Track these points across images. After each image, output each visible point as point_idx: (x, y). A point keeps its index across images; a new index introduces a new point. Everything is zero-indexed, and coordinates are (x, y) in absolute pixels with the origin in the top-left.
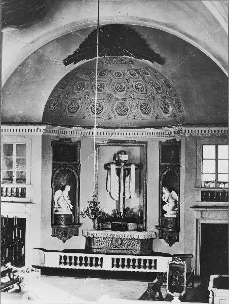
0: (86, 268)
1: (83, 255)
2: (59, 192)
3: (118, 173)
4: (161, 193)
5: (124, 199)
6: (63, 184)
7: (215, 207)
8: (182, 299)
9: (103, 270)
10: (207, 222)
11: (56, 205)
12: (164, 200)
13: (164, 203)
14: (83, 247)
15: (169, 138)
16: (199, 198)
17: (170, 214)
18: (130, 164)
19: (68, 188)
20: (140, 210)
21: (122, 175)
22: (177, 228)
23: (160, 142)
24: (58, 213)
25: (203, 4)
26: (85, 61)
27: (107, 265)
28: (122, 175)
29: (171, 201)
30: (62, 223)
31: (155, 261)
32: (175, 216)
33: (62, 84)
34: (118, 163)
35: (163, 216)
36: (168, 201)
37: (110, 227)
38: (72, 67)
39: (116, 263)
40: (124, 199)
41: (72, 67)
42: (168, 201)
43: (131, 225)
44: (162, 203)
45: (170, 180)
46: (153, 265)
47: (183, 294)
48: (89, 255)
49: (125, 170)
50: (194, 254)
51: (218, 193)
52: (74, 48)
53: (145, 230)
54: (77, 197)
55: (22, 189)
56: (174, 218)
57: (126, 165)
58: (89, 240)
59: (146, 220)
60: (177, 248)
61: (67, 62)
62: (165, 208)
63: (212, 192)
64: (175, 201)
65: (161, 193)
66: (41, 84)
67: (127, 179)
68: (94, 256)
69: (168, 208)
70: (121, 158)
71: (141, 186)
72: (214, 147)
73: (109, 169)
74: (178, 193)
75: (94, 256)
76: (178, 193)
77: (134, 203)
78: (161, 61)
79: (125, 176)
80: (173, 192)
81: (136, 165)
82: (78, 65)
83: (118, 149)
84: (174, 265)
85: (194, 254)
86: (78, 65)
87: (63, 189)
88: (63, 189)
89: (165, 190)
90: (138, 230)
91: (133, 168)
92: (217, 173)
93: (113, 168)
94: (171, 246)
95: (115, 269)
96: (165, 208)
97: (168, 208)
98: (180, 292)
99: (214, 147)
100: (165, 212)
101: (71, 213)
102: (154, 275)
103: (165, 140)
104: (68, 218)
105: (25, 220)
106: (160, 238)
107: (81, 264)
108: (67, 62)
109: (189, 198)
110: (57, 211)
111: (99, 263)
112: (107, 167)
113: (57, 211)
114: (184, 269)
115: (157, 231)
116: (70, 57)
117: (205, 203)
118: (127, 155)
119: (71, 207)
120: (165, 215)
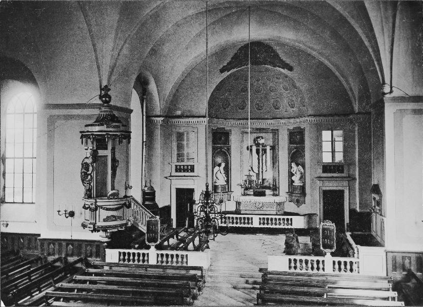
1: (235, 216)
2: (217, 168)
4: (290, 167)
5: (262, 172)
9: (253, 227)
10: (328, 189)
11: (215, 178)
13: (293, 175)
14: (234, 209)
15: (295, 126)
16: (320, 171)
19: (223, 165)
21: (261, 154)
22: (303, 193)
24: (217, 184)
26: (235, 70)
27: (256, 224)
29: (298, 173)
32: (302, 184)
33: (218, 88)
34: (258, 145)
36: (296, 173)
37: (252, 193)
38: (226, 74)
40: (262, 172)
41: (226, 74)
42: (296, 173)
43: (268, 192)
44: (291, 175)
45: (296, 156)
48: (238, 216)
49: (262, 150)
50: (318, 213)
56: (300, 186)
57: (263, 146)
58: (238, 203)
60: (304, 209)
62: (293, 178)
64: (301, 173)
65: (290, 167)
66: (220, 4)
67: (264, 156)
69: (296, 178)
70: (259, 142)
72: (330, 131)
73: (251, 150)
78: (290, 69)
82: (229, 73)
83: (255, 135)
85: (318, 213)
86: (229, 73)
87: (219, 165)
88: (219, 165)
89: (293, 165)
90: (274, 195)
95: (262, 226)
96: (293, 178)
97: (296, 178)
99: (330, 131)
101: (226, 183)
102: (290, 230)
104: (223, 188)
105: (194, 166)
109: (312, 172)
110: (216, 182)
111: (250, 221)
112: (250, 149)
113: (216, 182)
115: (287, 196)
118: (264, 140)
119: (226, 178)
120: (294, 184)
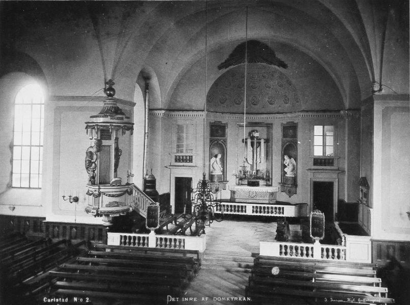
0: (235, 213)
1: (229, 204)
2: (213, 159)
3: (252, 145)
6: (216, 153)
7: (323, 169)
8: (322, 242)
10: (318, 180)
11: (212, 168)
12: (286, 164)
13: (285, 167)
14: (229, 197)
17: (289, 174)
18: (260, 140)
19: (220, 156)
20: (268, 171)
21: (255, 147)
23: (282, 124)
24: (213, 174)
25: (133, 91)
27: (249, 212)
28: (255, 147)
29: (290, 165)
30: (216, 181)
31: (283, 208)
34: (252, 138)
35: (284, 175)
36: (288, 165)
37: (246, 183)
39: (255, 209)
41: (224, 70)
42: (288, 165)
43: (261, 182)
45: (289, 149)
46: (281, 211)
47: (322, 238)
48: (233, 204)
49: (257, 143)
50: (309, 204)
51: (325, 159)
52: (226, 57)
53: (271, 185)
54: (225, 162)
55: (189, 156)
56: (292, 177)
58: (233, 193)
59: (272, 179)
61: (220, 68)
62: (286, 170)
63: (321, 159)
64: (294, 166)
67: (258, 149)
68: (237, 204)
69: (288, 170)
71: (268, 154)
73: (246, 143)
74: (296, 160)
75: (237, 204)
76: (296, 160)
77: (262, 167)
78: (284, 65)
79: (257, 148)
80: (292, 159)
81: (265, 140)
82: (227, 69)
84: (316, 216)
85: (309, 204)
87: (216, 156)
89: (286, 157)
90: (267, 185)
91: (262, 141)
92: (40, 146)
93: (249, 141)
94: (290, 197)
95: (255, 214)
96: (286, 170)
97: (288, 170)
98: (320, 236)
100: (286, 173)
103: (285, 123)
104: (219, 177)
106: (282, 191)
107: (231, 211)
108: (220, 68)
111: (244, 209)
114: (323, 219)
116: (222, 63)
117: (316, 167)
119: (222, 169)
